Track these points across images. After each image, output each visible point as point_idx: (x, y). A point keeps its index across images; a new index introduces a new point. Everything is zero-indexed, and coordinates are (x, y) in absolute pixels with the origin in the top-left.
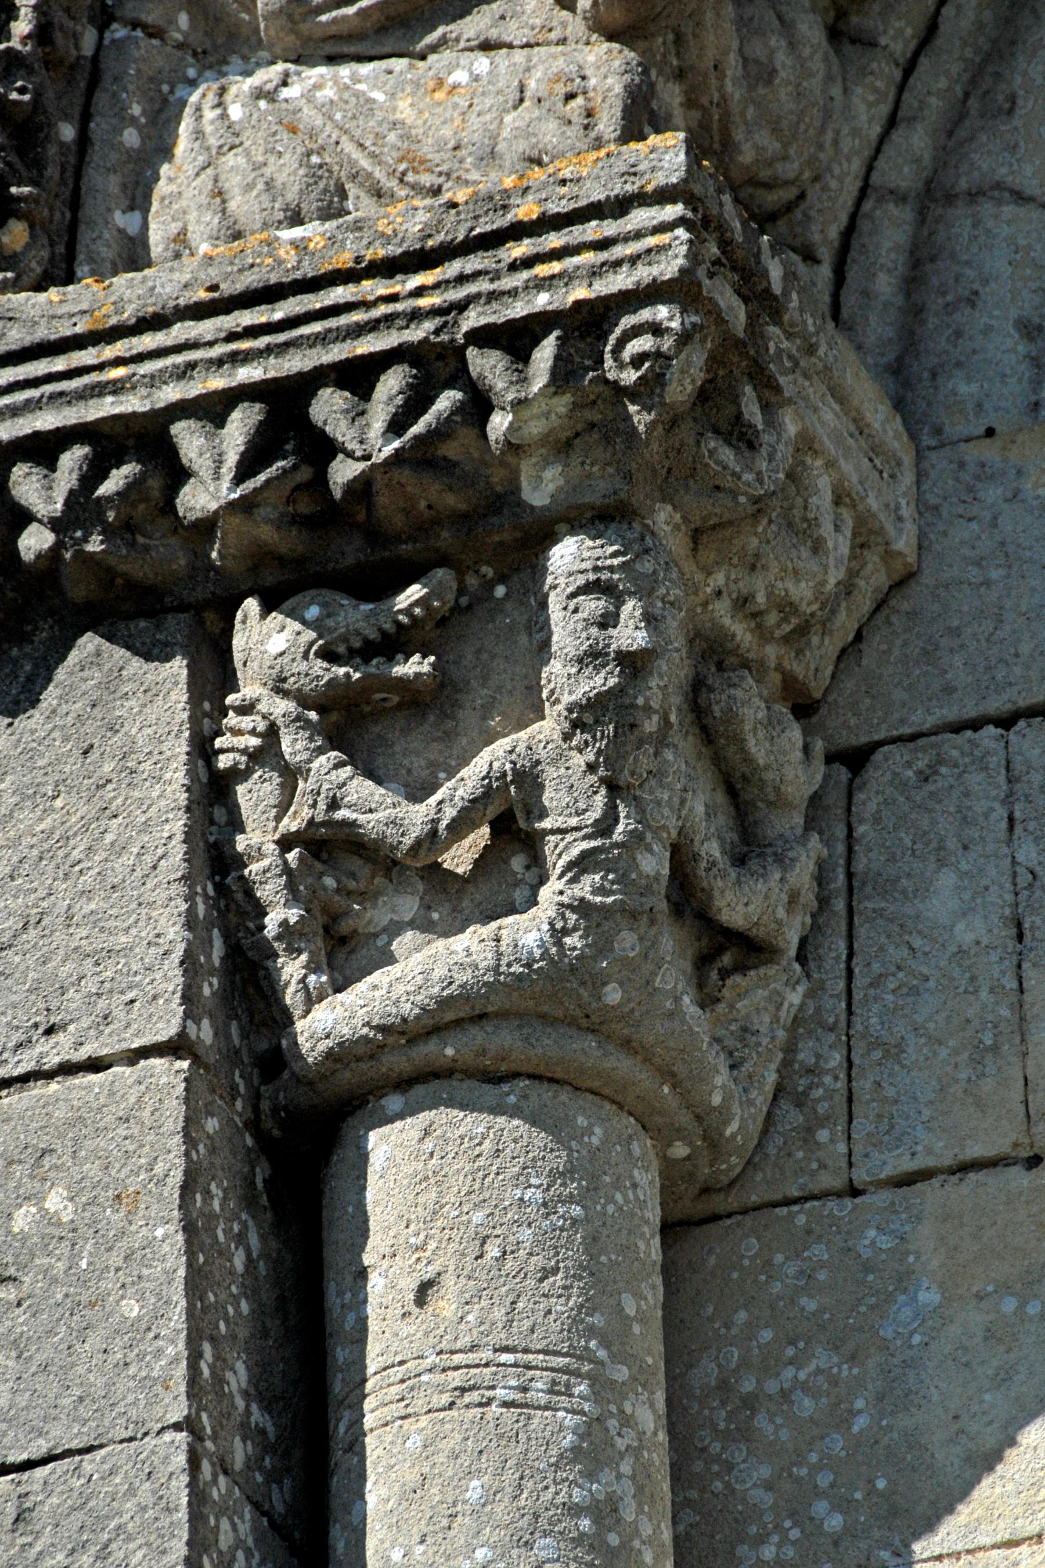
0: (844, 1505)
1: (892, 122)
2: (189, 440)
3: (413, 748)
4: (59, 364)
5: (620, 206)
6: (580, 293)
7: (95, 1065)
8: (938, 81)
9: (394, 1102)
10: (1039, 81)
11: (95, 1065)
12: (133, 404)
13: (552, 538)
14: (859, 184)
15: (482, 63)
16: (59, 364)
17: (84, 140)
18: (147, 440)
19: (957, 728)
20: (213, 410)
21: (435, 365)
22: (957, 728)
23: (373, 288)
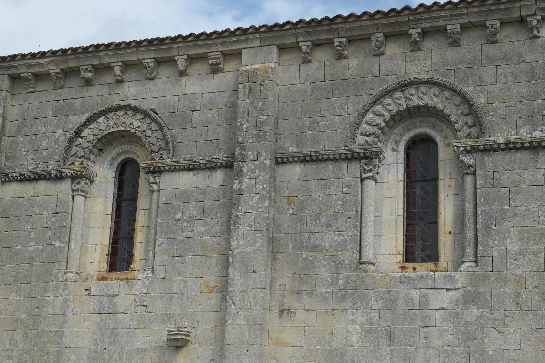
8: (387, 137)
18: (359, 153)
21: (371, 152)
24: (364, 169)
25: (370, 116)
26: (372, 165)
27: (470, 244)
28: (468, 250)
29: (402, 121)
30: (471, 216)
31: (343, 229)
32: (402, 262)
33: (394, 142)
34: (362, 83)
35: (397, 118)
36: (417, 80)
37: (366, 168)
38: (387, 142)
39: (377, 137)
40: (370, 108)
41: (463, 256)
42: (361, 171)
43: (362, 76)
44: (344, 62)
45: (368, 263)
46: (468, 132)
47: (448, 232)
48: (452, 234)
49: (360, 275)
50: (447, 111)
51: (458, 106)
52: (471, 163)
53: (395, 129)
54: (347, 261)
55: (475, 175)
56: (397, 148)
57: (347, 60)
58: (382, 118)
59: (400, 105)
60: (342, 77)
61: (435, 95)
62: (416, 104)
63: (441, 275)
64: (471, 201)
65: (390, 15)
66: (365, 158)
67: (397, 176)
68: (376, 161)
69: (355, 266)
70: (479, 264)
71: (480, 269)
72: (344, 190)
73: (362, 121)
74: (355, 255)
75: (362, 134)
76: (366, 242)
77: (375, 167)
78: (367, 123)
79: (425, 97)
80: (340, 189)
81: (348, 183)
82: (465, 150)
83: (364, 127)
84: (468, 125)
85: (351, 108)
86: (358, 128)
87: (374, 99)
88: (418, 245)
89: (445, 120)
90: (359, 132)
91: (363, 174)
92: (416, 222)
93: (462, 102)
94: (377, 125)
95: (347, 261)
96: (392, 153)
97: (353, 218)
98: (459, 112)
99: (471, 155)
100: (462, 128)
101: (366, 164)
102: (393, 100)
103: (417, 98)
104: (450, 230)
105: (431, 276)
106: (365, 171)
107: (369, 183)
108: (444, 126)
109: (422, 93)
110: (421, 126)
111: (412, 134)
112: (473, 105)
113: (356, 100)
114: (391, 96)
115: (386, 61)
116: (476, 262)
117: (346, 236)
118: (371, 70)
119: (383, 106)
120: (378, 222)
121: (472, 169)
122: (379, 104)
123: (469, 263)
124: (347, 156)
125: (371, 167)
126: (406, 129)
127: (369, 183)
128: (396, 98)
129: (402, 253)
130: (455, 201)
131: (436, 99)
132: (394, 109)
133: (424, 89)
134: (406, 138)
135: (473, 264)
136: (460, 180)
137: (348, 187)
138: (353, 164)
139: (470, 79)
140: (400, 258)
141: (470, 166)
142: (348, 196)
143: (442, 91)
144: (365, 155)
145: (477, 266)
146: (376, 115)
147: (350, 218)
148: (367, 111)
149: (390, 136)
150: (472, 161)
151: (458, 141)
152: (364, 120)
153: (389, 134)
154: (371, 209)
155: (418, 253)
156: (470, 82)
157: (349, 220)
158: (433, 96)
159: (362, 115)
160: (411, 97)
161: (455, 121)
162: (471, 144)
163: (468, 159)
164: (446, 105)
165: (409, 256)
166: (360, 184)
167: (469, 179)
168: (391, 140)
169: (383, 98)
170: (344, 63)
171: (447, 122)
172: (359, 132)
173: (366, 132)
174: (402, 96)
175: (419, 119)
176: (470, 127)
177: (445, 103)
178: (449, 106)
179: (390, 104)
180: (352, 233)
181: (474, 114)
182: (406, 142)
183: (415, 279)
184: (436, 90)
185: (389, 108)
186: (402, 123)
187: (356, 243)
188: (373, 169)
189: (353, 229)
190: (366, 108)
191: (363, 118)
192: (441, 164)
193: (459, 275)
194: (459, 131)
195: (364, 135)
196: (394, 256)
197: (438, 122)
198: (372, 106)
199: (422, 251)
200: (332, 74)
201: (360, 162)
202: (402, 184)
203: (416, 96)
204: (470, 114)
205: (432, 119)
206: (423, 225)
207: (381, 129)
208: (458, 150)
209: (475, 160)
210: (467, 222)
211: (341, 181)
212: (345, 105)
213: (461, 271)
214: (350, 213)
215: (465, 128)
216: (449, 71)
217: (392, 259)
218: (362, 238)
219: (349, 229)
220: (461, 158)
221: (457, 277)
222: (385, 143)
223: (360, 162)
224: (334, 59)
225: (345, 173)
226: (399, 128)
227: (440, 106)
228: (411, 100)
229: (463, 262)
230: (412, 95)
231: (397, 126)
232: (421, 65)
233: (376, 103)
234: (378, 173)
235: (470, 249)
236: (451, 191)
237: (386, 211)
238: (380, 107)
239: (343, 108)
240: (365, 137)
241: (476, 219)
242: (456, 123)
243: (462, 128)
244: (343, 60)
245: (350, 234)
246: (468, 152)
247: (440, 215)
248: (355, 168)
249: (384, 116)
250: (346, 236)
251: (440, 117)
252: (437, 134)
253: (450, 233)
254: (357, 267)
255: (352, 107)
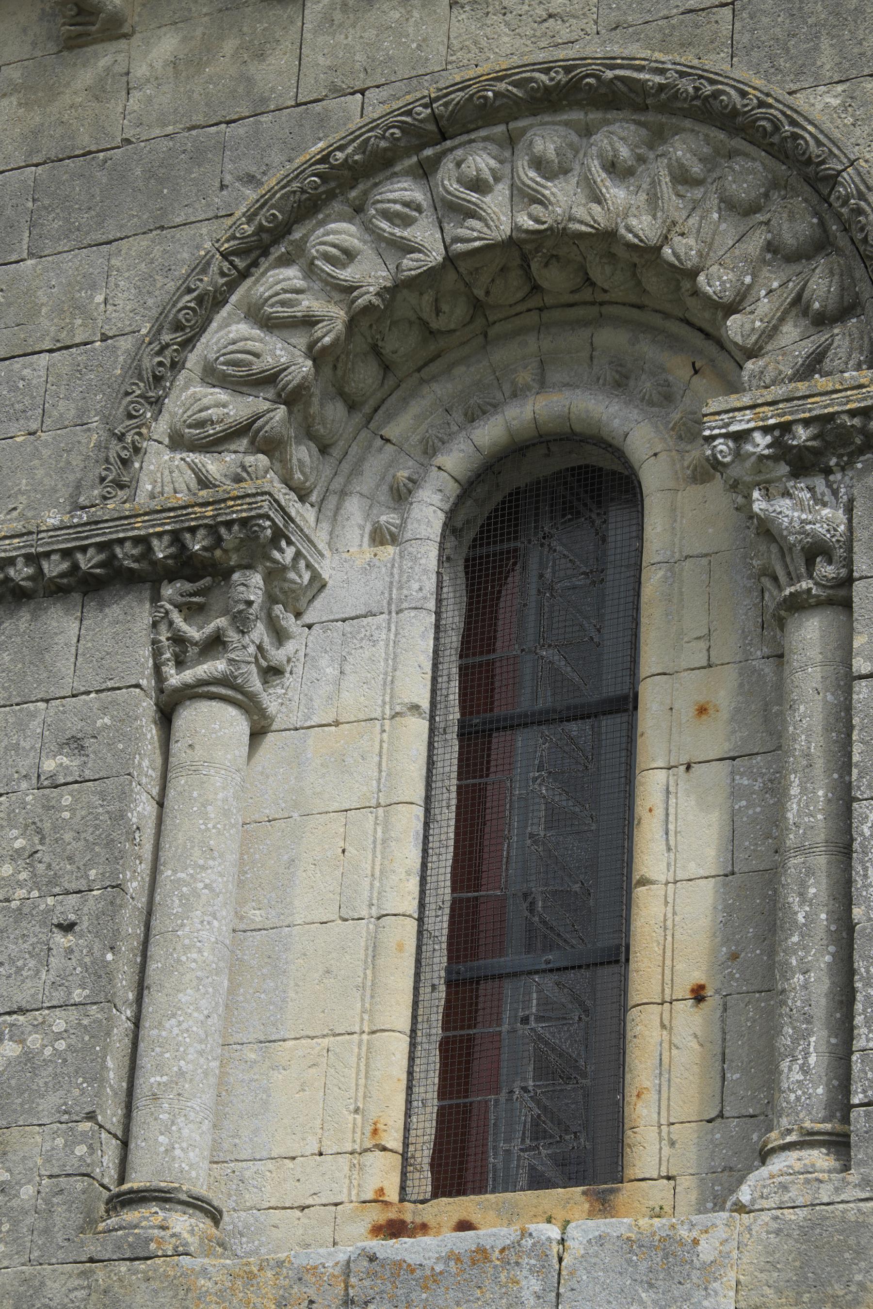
0: (286, 802)
1: (336, 474)
2: (155, 542)
3: (200, 619)
4: (118, 523)
5: (257, 494)
6: (244, 515)
7: (119, 688)
8: (346, 467)
9: (188, 703)
10: (4, 1219)
11: (119, 688)
12: (142, 533)
13: (234, 572)
14: (684, 325)
15: (233, 456)
16: (118, 523)
17: (141, 468)
18: (143, 541)
19: (332, 621)
20: (159, 535)
21: (212, 529)
22: (332, 621)
23: (197, 509)
24: (179, 640)
25: (229, 332)
26: (225, 612)
27: (805, 1036)
28: (792, 1075)
29: (433, 368)
30: (821, 861)
31: (21, 998)
32: (393, 1195)
33: (383, 496)
34: (198, 157)
35: (399, 344)
36: (502, 86)
37: (193, 632)
38: (343, 494)
39: (271, 446)
40: (232, 286)
41: (764, 1115)
42: (157, 653)
43: (198, 118)
44: (105, 58)
45: (162, 1197)
46: (807, 347)
47: (683, 989)
48: (713, 1001)
49: (100, 1273)
50: (683, 248)
51: (752, 209)
52: (820, 529)
53: (390, 417)
54: (27, 1191)
55: (847, 605)
56: (402, 526)
57: (123, 44)
58: (301, 340)
59: (406, 248)
60: (85, 141)
61: (612, 167)
62: (505, 229)
63: (601, 1240)
64: (819, 764)
65: (590, 230)
66: (185, 566)
67: (390, 683)
68: (252, 586)
69: (78, 1219)
70: (858, 1154)
71: (865, 1182)
72: (49, 765)
73: (176, 366)
74: (81, 1150)
75: (177, 442)
76: (159, 1069)
77: (242, 623)
78: (212, 376)
79: (552, 189)
80: (25, 764)
81: (73, 726)
82: (782, 450)
83: (194, 397)
84: (805, 313)
85: (125, 300)
86: (157, 404)
87: (249, 229)
88: (512, 1105)
89: (683, 331)
90: (161, 428)
91: (170, 670)
92: (510, 960)
93: (775, 184)
94: (268, 380)
95: (27, 1191)
96: (368, 552)
97: (85, 924)
98: (755, 244)
99: (820, 483)
100: (772, 332)
101: (193, 611)
102: (369, 228)
103: (502, 198)
104: (698, 976)
105: (540, 1250)
106: (182, 651)
107: (214, 726)
108: (678, 368)
109: (538, 164)
110: (543, 384)
111: (490, 433)
112: (833, 179)
113: (157, 251)
114: (359, 209)
115: (338, 16)
116: (840, 1144)
117: (34, 1040)
118: (250, 81)
119: (310, 271)
120: (255, 951)
121: (826, 570)
122: (285, 261)
123: (794, 1154)
124: (75, 567)
125: (221, 622)
126: (458, 416)
127: (214, 726)
128: (387, 215)
129: (394, 1141)
130: (735, 793)
131: (617, 194)
132: (371, 275)
133: (546, 140)
134: (456, 460)
135: (819, 1159)
136: (768, 669)
137: (75, 744)
138: (115, 611)
139: (825, 43)
140: (382, 1172)
141: (816, 551)
142: (67, 800)
143: (658, 137)
144: (183, 547)
145: (846, 1168)
146: (269, 324)
147: (68, 928)
148: (211, 303)
149: (361, 460)
150: (826, 520)
151: (734, 401)
152: (193, 359)
153: (354, 450)
154: (207, 876)
155: (506, 1140)
156: (827, 60)
157: (62, 940)
158: (600, 175)
159: (178, 327)
160: (474, 197)
161: (729, 296)
162: (820, 407)
163: (800, 510)
164: (679, 216)
165: (457, 1162)
166: (152, 732)
167: (810, 634)
168: (367, 481)
169: (310, 224)
170: (103, 62)
171: (698, 340)
172: (161, 428)
173: (201, 424)
174: (418, 195)
175: (532, 344)
176: (822, 320)
177: (673, 203)
178: (694, 221)
179: (349, 255)
180: (73, 1014)
181: (842, 241)
182: (453, 489)
183: (436, 1278)
184: (619, 138)
185: (346, 274)
186: (434, 378)
187: (98, 1078)
188: (232, 636)
189: (78, 995)
190: (207, 282)
191: (188, 344)
192: (653, 583)
193: (721, 1232)
194: (753, 353)
195: (195, 446)
196: (344, 1162)
197: (648, 349)
198: (244, 275)
199: (538, 1133)
200: (36, 133)
201: (156, 598)
202: (419, 726)
203: (502, 190)
204: (820, 245)
205: (611, 338)
206: (548, 981)
207: (293, 398)
208: (738, 454)
209: (849, 510)
210: (794, 899)
211: (33, 715)
212: (93, 287)
213: (740, 1208)
214: (73, 899)
215: (790, 332)
216: (701, 17)
217: (335, 1180)
218: (142, 1046)
219: (58, 997)
220: (759, 505)
221: (707, 1250)
222: (332, 500)
223: (156, 598)
224: (52, 47)
225: (65, 666)
226: (415, 408)
227: (643, 226)
228: (473, 215)
229: (764, 1156)
230: (478, 185)
231: (405, 401)
232: (540, 12)
233: (266, 253)
234: (272, 673)
235: (805, 1070)
236: (713, 738)
237: (311, 895)
238: (292, 275)
239: (80, 308)
240: (191, 457)
241: (849, 882)
242: (732, 309)
243: (772, 332)
244: (98, 47)
245: (59, 1025)
246: (802, 464)
247: (640, 892)
248: (123, 636)
249: (309, 322)
250: (34, 1040)
251: (657, 320)
252: (634, 414)
253: (698, 995)
254: (89, 1224)
255: (126, 295)
